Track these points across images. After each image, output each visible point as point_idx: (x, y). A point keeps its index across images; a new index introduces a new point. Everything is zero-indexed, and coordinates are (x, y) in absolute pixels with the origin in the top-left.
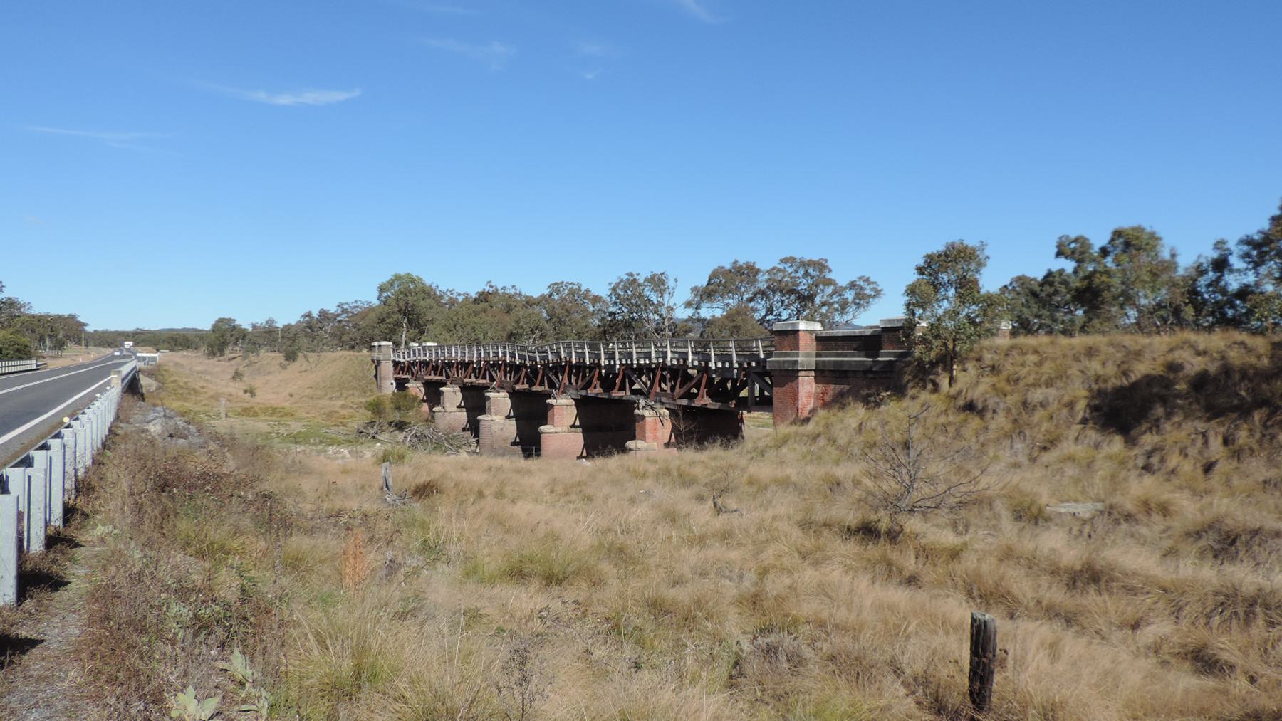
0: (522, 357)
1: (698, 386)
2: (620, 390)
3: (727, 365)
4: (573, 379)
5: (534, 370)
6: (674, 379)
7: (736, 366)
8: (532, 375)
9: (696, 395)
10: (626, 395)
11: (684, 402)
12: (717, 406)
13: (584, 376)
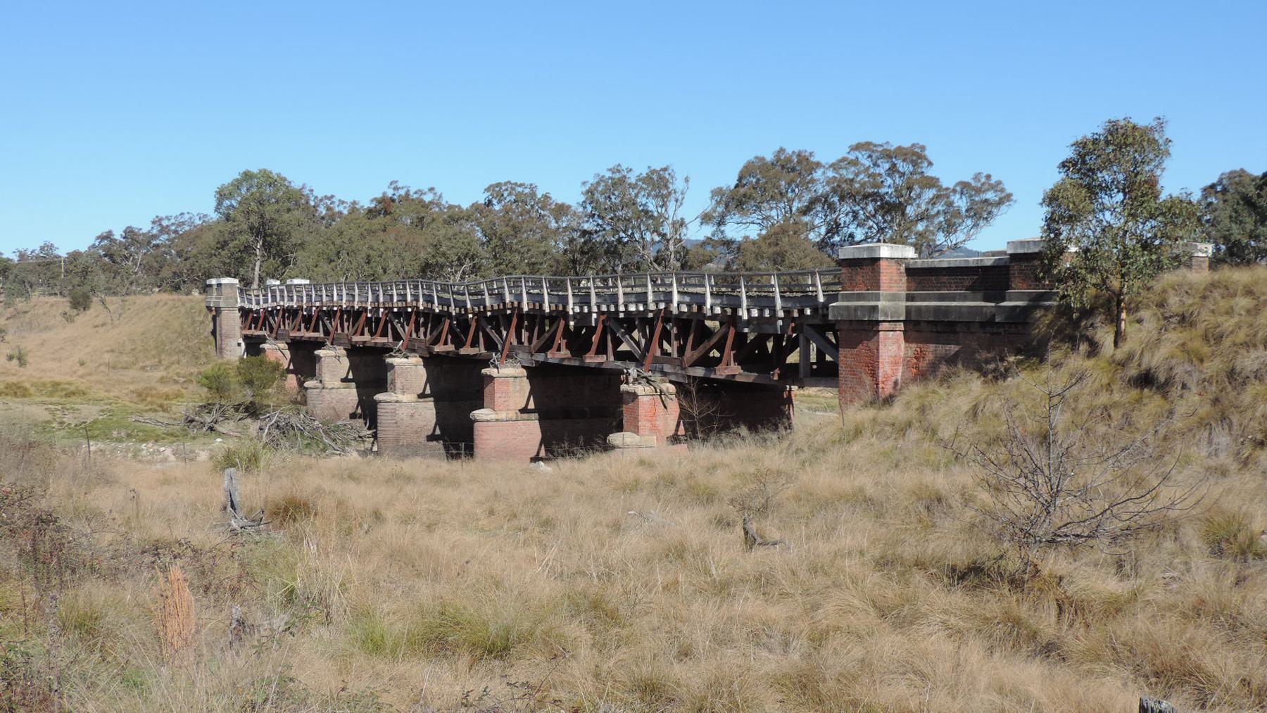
1: (720, 347)
2: (598, 352)
3: (586, 310)
5: (463, 323)
6: (682, 335)
8: (460, 329)
9: (718, 361)
11: (699, 372)
12: (750, 377)
13: (541, 332)
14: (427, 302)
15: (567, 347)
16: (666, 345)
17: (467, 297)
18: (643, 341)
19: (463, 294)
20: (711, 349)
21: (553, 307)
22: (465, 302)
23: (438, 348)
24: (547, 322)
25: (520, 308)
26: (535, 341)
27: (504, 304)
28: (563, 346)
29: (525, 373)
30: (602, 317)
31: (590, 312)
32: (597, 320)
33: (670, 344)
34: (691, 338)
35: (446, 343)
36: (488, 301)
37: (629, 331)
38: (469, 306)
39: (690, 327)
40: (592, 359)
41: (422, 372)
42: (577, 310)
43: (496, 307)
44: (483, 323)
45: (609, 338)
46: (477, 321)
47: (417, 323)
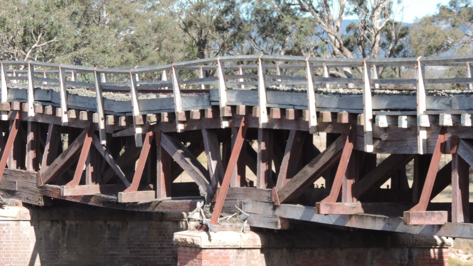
0: (76, 104)
1: (329, 172)
2: (143, 186)
3: (404, 123)
4: (30, 156)
5: (120, 141)
6: (274, 154)
7: (425, 121)
8: (116, 153)
9: (323, 193)
10: (159, 196)
11: (296, 212)
12: (376, 224)
13: (57, 150)
14: (44, 103)
15: (356, 194)
16: (248, 171)
17: (96, 94)
18: (214, 164)
19: (127, 91)
20: (315, 177)
21: (277, 115)
22: (129, 103)
23: (71, 191)
24: (65, 138)
25: (22, 112)
26: (43, 167)
27: (216, 109)
28: (348, 192)
29: (257, 240)
30: (442, 138)
31: (414, 128)
32: (427, 143)
33: (255, 170)
34: (287, 157)
35: (83, 182)
36: (180, 105)
37: (193, 153)
38: (136, 112)
39: (286, 142)
40: (130, 195)
41: (28, 234)
42: (383, 122)
43: (196, 115)
44: (167, 144)
45: (160, 165)
46: (153, 142)
47: (248, 158)
